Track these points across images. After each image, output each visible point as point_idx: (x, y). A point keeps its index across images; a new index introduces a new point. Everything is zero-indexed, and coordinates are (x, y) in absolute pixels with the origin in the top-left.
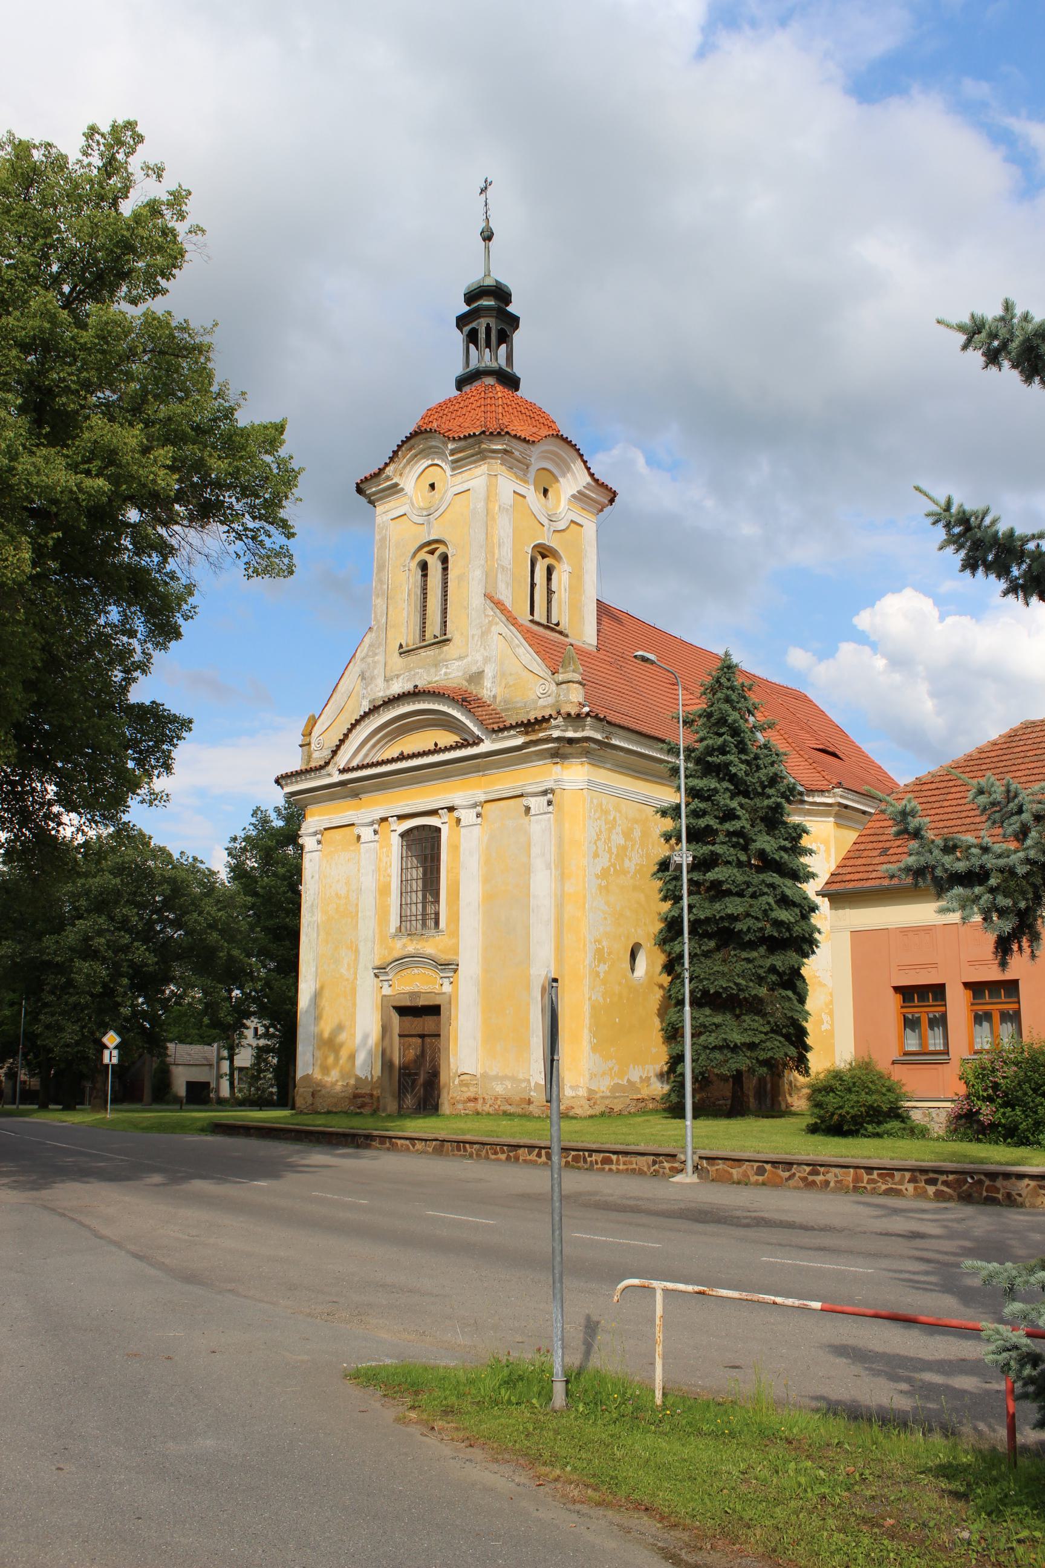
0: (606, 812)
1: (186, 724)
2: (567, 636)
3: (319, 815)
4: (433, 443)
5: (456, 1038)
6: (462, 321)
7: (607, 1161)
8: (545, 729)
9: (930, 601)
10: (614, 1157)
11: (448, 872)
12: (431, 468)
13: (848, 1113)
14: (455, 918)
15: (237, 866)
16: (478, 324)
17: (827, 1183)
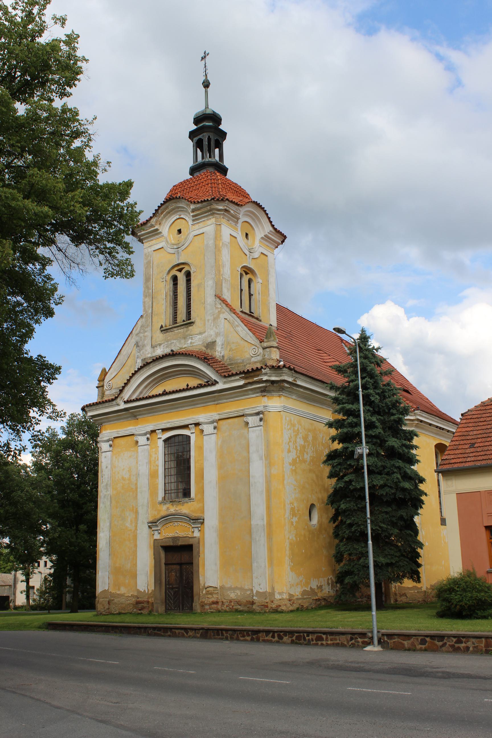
0: (294, 425)
1: (58, 370)
2: (260, 321)
3: (110, 429)
4: (181, 205)
5: (204, 565)
6: (192, 135)
7: (320, 639)
8: (258, 376)
9: (403, 310)
10: (324, 636)
11: (195, 463)
12: (178, 220)
13: (466, 604)
14: (201, 491)
15: (37, 462)
16: (203, 136)
17: (468, 648)
